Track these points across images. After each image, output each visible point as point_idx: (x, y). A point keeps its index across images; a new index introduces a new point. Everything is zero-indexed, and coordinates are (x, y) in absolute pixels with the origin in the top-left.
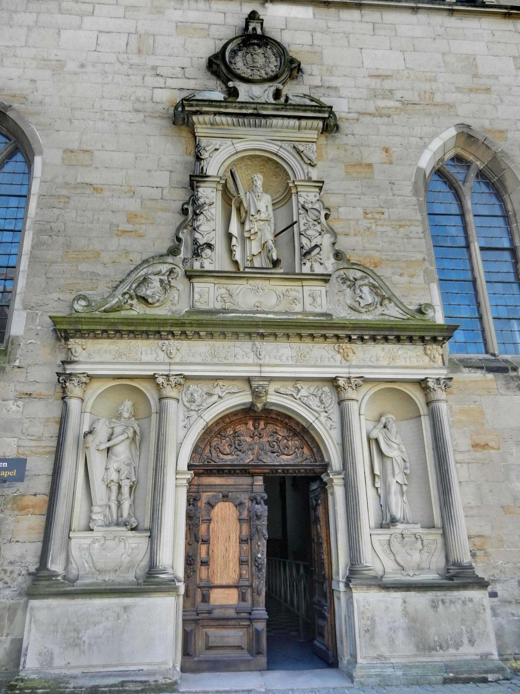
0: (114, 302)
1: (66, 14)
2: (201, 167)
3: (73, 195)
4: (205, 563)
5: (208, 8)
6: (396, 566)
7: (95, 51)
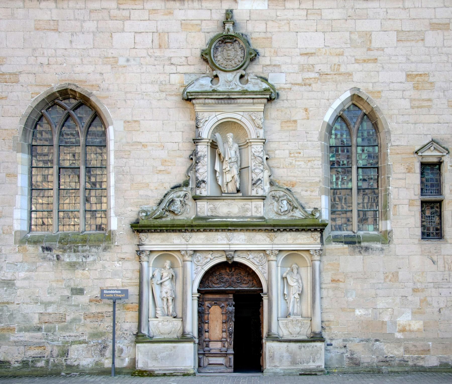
0: (158, 213)
1: (114, 20)
4: (208, 332)
5: (200, 6)
7: (134, 48)
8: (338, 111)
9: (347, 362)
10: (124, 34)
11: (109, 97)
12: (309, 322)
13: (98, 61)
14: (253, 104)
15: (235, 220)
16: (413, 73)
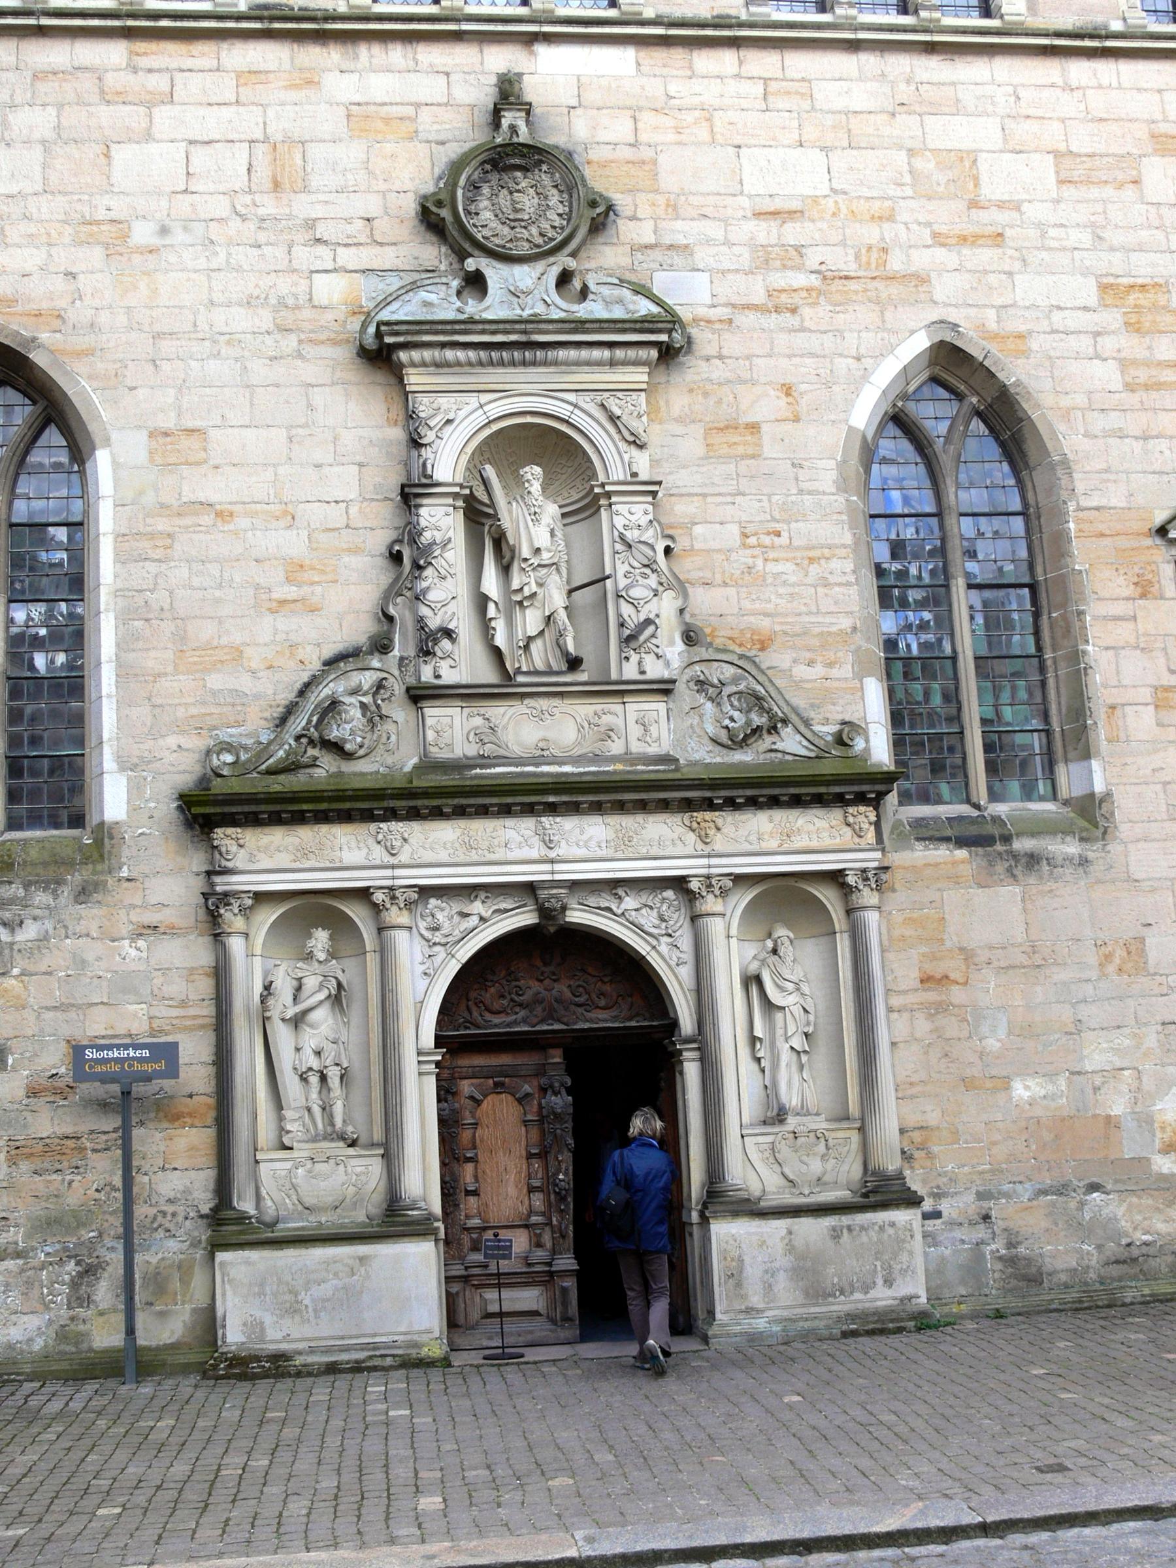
0: (281, 753)
2: (421, 461)
3: (177, 529)
4: (475, 1193)
5: (411, 64)
6: (784, 1182)
7: (186, 191)
8: (891, 397)
9: (997, 1275)
10: (153, 148)
11: (99, 353)
12: (855, 1137)
13: (60, 234)
14: (612, 363)
15: (567, 769)
16: (1120, 280)
